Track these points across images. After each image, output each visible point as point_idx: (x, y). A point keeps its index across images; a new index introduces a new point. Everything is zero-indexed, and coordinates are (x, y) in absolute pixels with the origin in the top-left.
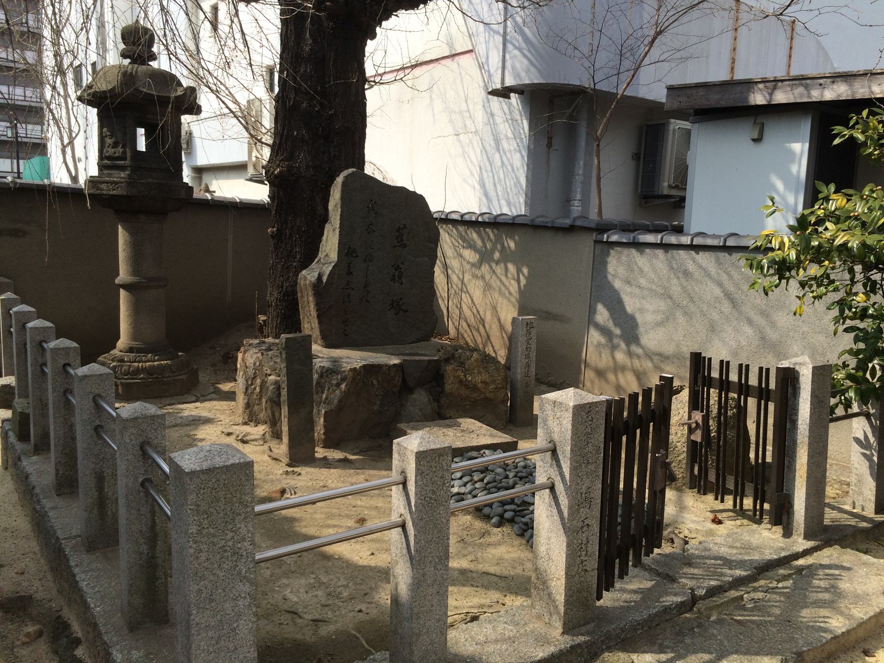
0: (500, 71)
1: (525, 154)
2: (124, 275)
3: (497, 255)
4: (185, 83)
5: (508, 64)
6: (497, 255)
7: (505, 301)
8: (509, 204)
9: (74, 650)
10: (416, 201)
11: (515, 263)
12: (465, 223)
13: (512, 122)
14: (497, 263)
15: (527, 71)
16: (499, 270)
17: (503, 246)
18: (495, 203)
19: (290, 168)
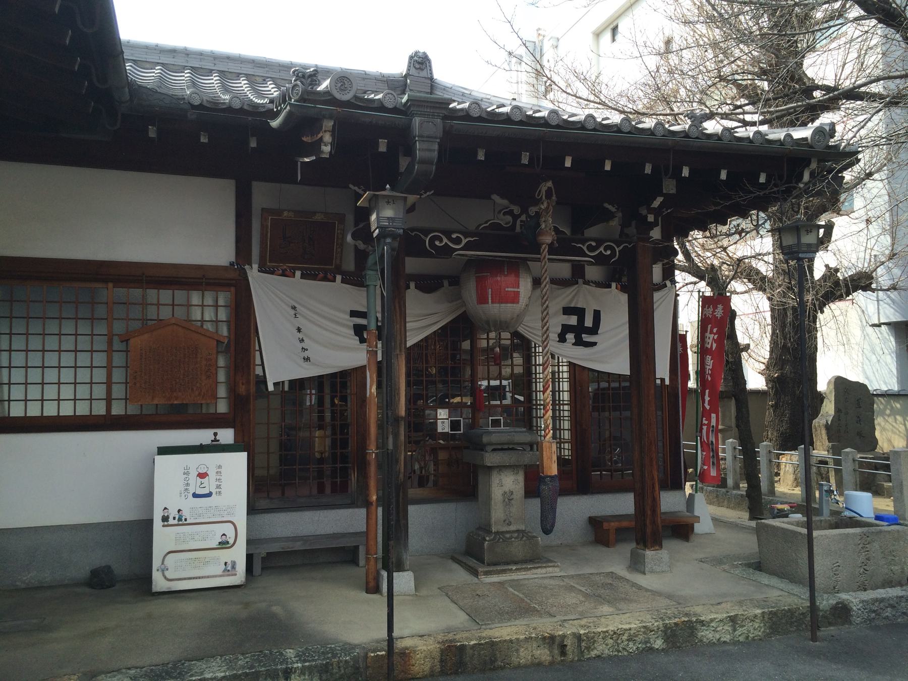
0: (876, 315)
1: (894, 356)
2: (498, 403)
3: (888, 412)
4: (349, 421)
5: (881, 311)
6: (888, 412)
7: (896, 437)
8: (885, 383)
9: (409, 255)
10: (861, 387)
11: (900, 415)
12: (888, 395)
13: (887, 341)
14: (889, 416)
15: (894, 315)
16: (891, 420)
17: (892, 407)
18: (876, 383)
19: (782, 374)
